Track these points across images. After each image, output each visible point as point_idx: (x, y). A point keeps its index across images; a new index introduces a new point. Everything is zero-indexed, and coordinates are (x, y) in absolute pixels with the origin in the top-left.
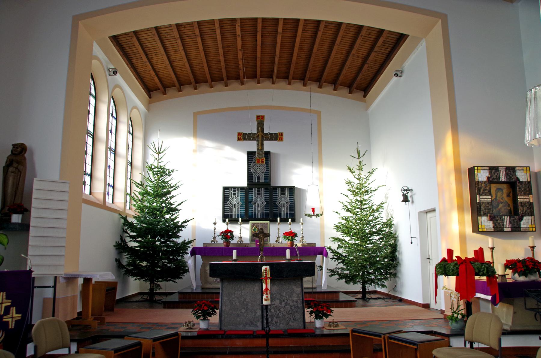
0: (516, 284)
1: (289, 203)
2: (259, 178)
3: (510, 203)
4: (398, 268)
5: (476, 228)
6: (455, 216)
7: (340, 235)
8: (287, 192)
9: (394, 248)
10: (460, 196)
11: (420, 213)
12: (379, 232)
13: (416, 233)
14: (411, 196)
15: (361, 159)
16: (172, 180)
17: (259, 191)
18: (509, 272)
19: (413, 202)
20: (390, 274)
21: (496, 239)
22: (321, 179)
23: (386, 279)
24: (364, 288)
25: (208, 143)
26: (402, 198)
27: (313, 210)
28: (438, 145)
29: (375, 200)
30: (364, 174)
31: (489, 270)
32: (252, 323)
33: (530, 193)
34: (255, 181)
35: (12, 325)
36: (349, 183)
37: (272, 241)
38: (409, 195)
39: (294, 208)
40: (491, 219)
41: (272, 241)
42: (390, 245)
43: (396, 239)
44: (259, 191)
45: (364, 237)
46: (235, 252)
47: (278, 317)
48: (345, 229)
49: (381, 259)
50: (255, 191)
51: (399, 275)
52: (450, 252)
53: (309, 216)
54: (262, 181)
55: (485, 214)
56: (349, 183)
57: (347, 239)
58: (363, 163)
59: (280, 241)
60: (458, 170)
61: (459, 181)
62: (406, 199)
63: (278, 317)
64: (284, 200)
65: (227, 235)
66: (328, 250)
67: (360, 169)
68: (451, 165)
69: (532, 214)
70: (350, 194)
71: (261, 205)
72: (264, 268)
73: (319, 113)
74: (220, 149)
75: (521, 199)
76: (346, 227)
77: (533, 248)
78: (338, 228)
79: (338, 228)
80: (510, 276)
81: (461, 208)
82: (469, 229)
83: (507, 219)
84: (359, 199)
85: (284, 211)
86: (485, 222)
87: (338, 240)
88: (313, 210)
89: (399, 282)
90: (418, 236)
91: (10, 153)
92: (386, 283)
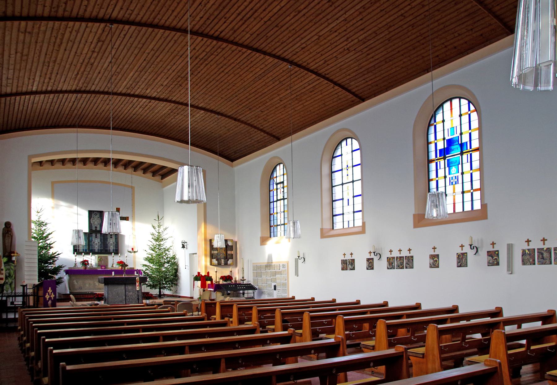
0: (223, 285)
1: (115, 243)
2: (96, 227)
3: (225, 254)
4: (178, 281)
5: (211, 264)
6: (203, 258)
7: (147, 263)
8: (114, 237)
9: (177, 270)
10: (206, 250)
11: (190, 254)
12: (168, 262)
13: (188, 264)
14: (186, 245)
15: (159, 222)
16: (48, 229)
17: (96, 235)
18: (221, 280)
19: (187, 248)
20: (174, 284)
21: (218, 268)
22: (133, 229)
23: (172, 286)
24: (160, 292)
25: (62, 203)
26: (182, 246)
27: (133, 249)
28: (199, 227)
29: (166, 244)
30: (161, 230)
31: (211, 279)
32: (121, 302)
33: (232, 250)
34: (94, 229)
35: (53, 299)
36: (153, 234)
37: (110, 267)
38: (185, 245)
39: (118, 246)
40: (217, 260)
41: (110, 267)
42: (175, 269)
43: (177, 266)
44: (96, 235)
45: (161, 265)
46: (113, 273)
47: (132, 299)
48: (150, 260)
49: (170, 275)
50: (94, 235)
51: (179, 284)
52: (199, 273)
53: (130, 252)
54: (98, 229)
55: (214, 258)
56: (153, 234)
57: (151, 265)
58: (161, 224)
59: (114, 266)
60: (205, 240)
61: (205, 244)
62: (183, 247)
63: (132, 299)
64: (111, 241)
65: (85, 263)
66: (142, 272)
67: (159, 226)
68: (203, 237)
69: (232, 258)
70: (153, 240)
71: (98, 244)
72: (137, 278)
73: (133, 188)
74: (71, 207)
75: (229, 252)
76: (152, 259)
77: (231, 271)
78: (147, 259)
79: (147, 259)
80: (221, 282)
81: (206, 255)
82: (209, 264)
83: (223, 260)
84: (158, 244)
85: (112, 248)
86: (215, 261)
87: (146, 266)
88: (133, 249)
89: (179, 288)
90: (189, 265)
91: (4, 226)
92: (172, 288)
